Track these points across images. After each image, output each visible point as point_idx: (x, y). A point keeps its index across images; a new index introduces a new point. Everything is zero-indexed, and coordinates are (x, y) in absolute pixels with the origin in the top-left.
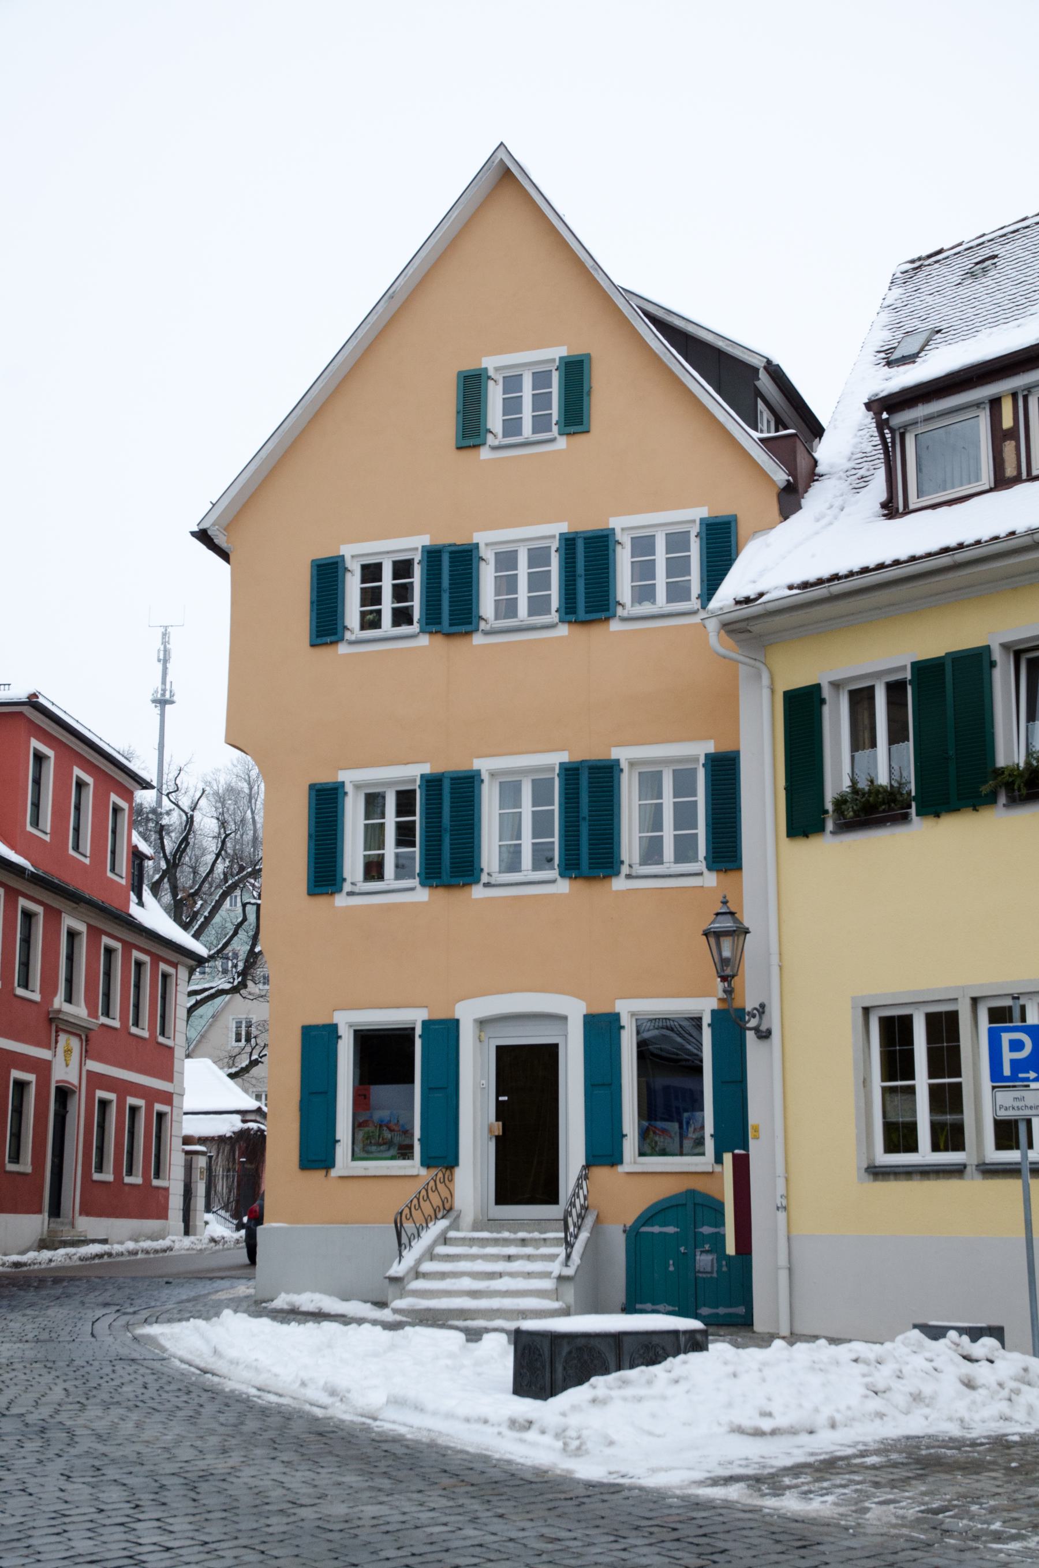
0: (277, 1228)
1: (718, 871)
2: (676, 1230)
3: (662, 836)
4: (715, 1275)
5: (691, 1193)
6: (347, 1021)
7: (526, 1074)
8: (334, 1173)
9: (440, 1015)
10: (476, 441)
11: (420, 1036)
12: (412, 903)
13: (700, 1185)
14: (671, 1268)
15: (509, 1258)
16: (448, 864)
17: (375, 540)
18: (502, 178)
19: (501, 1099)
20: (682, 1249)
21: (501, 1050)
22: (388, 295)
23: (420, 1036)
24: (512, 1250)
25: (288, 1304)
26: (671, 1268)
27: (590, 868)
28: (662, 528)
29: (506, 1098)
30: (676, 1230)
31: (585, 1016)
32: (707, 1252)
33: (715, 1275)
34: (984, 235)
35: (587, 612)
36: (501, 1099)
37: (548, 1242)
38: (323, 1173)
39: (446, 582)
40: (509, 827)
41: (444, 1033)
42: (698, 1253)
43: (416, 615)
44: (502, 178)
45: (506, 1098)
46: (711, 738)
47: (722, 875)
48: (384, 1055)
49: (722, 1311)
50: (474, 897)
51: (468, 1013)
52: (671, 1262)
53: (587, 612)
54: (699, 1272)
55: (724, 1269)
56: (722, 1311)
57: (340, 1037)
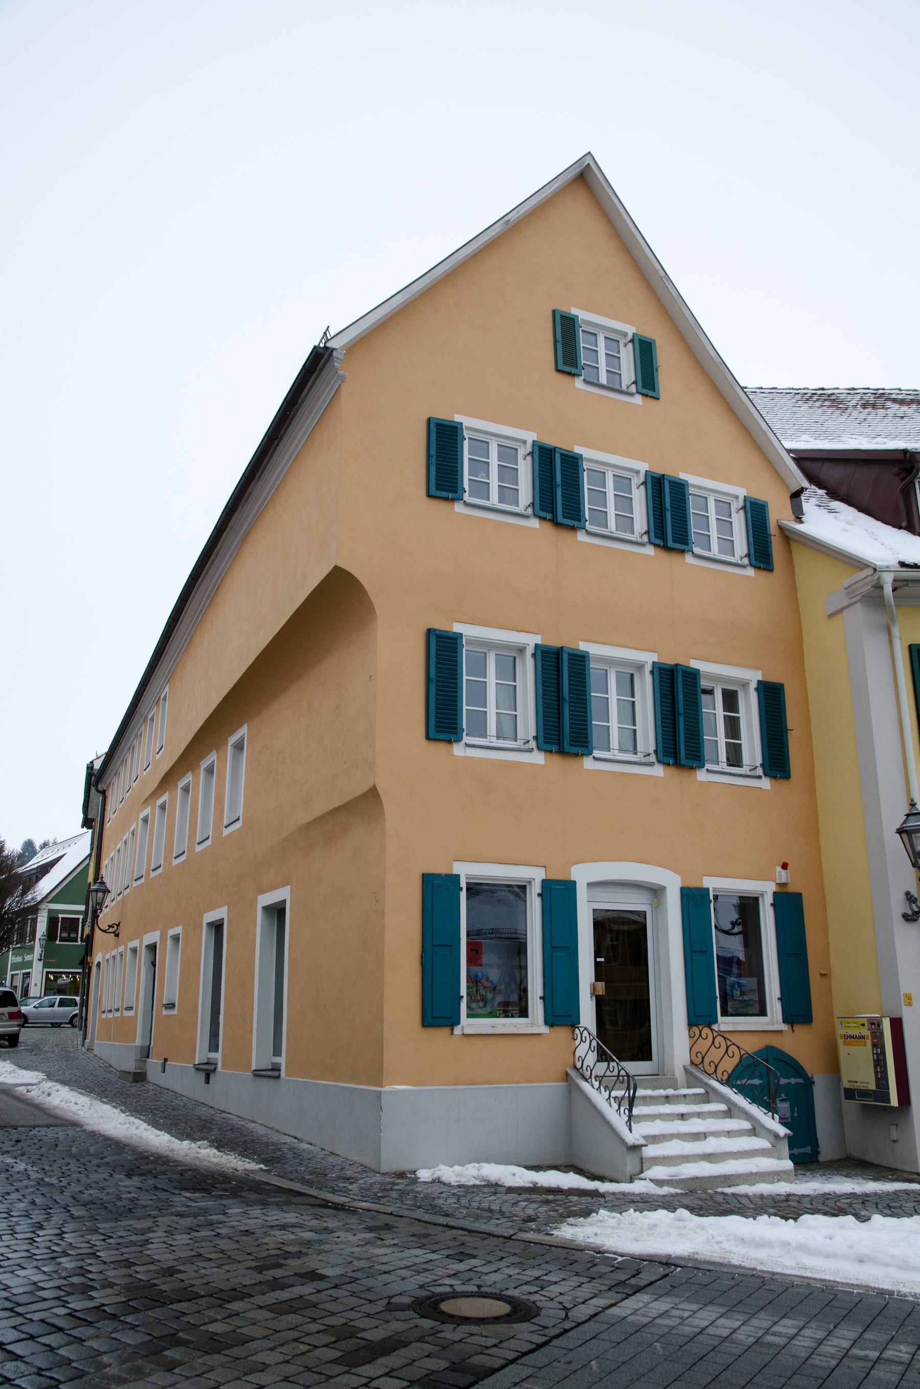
0: (404, 1091)
4: (789, 1120)
5: (769, 1049)
8: (457, 1030)
12: (530, 764)
14: (796, 1114)
15: (682, 1117)
16: (568, 732)
18: (584, 179)
19: (598, 960)
22: (506, 218)
23: (461, 889)
24: (683, 1108)
25: (531, 1182)
29: (603, 960)
31: (682, 889)
33: (789, 1120)
34: (837, 389)
36: (598, 960)
37: (688, 1098)
38: (447, 1031)
40: (625, 717)
42: (778, 1102)
44: (584, 179)
45: (603, 960)
47: (773, 780)
50: (699, 779)
53: (437, 489)
55: (796, 1114)
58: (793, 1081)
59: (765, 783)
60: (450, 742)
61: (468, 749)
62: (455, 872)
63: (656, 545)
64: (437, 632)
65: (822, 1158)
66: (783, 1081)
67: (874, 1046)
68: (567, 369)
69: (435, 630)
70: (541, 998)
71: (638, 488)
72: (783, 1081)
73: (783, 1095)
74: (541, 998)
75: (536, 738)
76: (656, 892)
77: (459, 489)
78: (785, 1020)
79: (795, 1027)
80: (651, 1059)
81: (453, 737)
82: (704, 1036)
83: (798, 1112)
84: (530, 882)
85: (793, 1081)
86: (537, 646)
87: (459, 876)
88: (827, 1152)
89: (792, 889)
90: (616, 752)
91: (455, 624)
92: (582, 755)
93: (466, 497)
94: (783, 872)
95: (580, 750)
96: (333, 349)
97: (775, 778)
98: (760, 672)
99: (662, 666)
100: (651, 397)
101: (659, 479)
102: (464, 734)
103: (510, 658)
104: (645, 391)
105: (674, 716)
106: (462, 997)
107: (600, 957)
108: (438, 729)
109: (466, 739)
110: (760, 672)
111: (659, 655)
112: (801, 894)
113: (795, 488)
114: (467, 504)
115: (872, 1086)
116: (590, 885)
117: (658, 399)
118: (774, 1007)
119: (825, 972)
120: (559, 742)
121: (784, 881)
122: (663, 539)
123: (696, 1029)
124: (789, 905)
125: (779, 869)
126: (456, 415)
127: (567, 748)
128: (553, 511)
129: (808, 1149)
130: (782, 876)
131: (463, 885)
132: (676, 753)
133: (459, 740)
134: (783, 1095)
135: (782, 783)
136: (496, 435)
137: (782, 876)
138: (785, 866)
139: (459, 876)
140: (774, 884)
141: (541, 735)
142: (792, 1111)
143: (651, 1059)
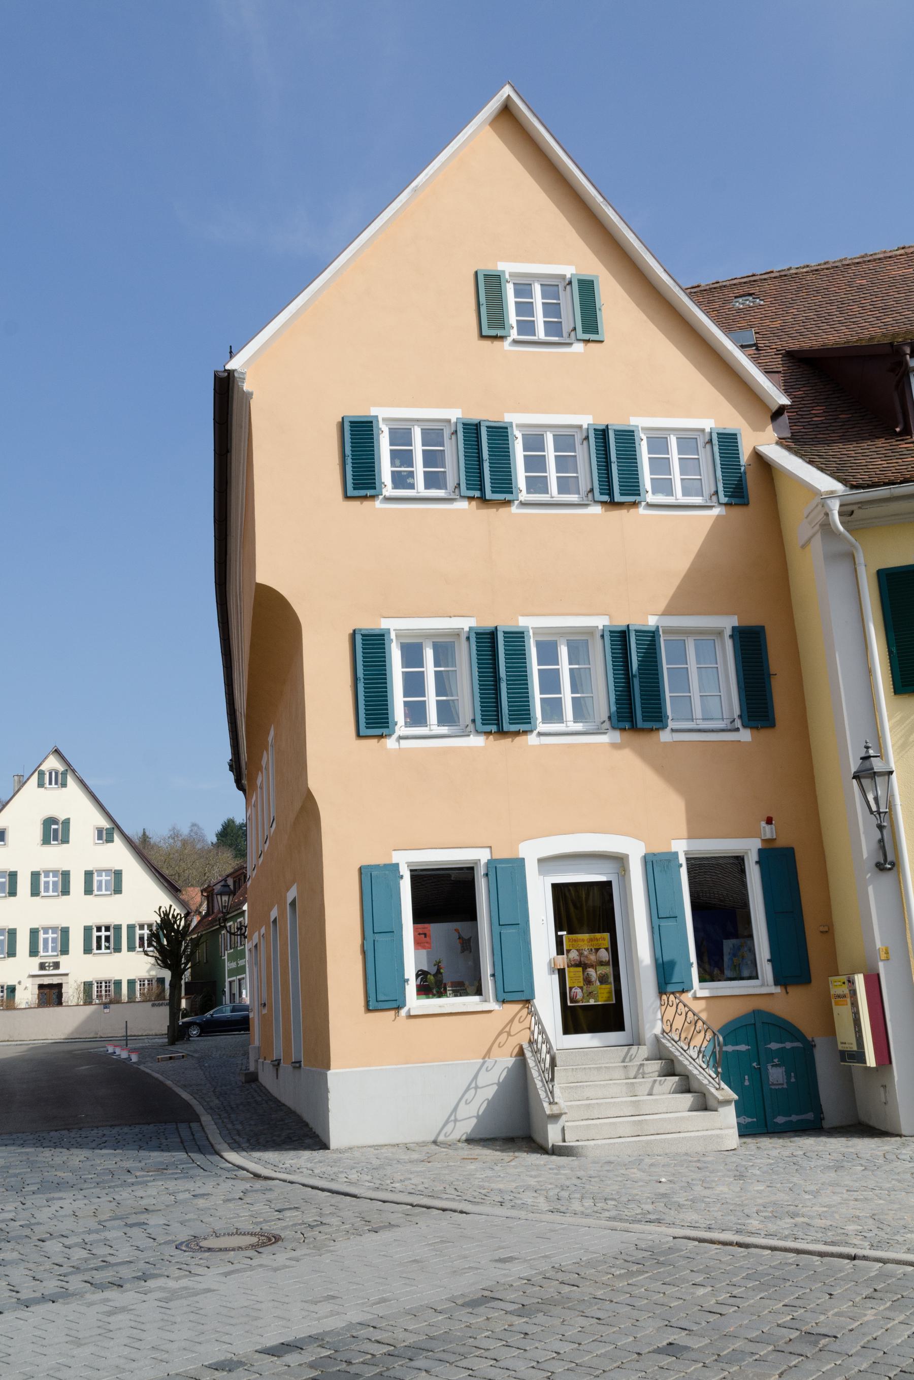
1: (751, 728)
2: (747, 1047)
3: (437, 696)
4: (785, 1086)
5: (756, 1013)
6: (406, 860)
7: (586, 909)
8: (403, 1012)
9: (502, 853)
10: (500, 333)
11: (681, 865)
13: (763, 1005)
14: (747, 1083)
16: (507, 711)
17: (407, 406)
19: (560, 933)
20: (754, 1064)
21: (556, 887)
26: (747, 1083)
27: (619, 721)
28: (420, 423)
30: (747, 1047)
32: (776, 1066)
33: (785, 1086)
34: (875, 254)
35: (355, 489)
36: (560, 933)
39: (613, 457)
41: (509, 872)
43: (451, 481)
46: (735, 614)
47: (755, 731)
48: (445, 896)
49: (794, 1118)
51: (531, 852)
52: (746, 1077)
53: (355, 489)
54: (773, 1084)
55: (793, 1080)
56: (794, 1118)
57: (757, 862)
58: (788, 1045)
59: (745, 735)
60: (381, 736)
61: (542, 738)
62: (673, 850)
63: (603, 503)
64: (363, 632)
65: (826, 1124)
66: (774, 1046)
67: (852, 1004)
68: (493, 332)
69: (360, 630)
70: (769, 960)
71: (705, 447)
72: (774, 1046)
73: (776, 1060)
74: (769, 960)
75: (740, 717)
76: (620, 861)
77: (642, 492)
78: (777, 983)
79: (789, 989)
80: (624, 1030)
81: (385, 731)
82: (671, 1003)
83: (796, 1077)
84: (476, 863)
85: (788, 1045)
86: (734, 628)
87: (397, 865)
88: (831, 1116)
89: (781, 843)
90: (571, 724)
91: (383, 620)
92: (658, 729)
93: (524, 496)
94: (768, 827)
95: (655, 725)
96: (234, 371)
97: (757, 728)
98: (736, 617)
99: (612, 629)
100: (593, 341)
101: (603, 431)
102: (669, 721)
103: (579, 644)
104: (587, 336)
105: (629, 679)
106: (692, 964)
107: (561, 930)
108: (369, 725)
109: (671, 724)
110: (736, 617)
111: (610, 618)
112: (793, 849)
113: (774, 408)
114: (651, 506)
115: (855, 1048)
116: (541, 861)
117: (602, 342)
118: (766, 969)
119: (826, 929)
120: (498, 722)
121: (768, 836)
122: (609, 494)
123: (664, 997)
124: (779, 863)
125: (763, 824)
126: (631, 418)
127: (507, 727)
128: (482, 489)
129: (810, 1116)
130: (768, 831)
131: (682, 860)
132: (632, 717)
133: (664, 727)
134: (776, 1060)
135: (764, 734)
136: (418, 420)
137: (768, 831)
138: (769, 821)
139: (397, 865)
140: (759, 840)
141: (745, 713)
142: (788, 1077)
143: (624, 1030)
